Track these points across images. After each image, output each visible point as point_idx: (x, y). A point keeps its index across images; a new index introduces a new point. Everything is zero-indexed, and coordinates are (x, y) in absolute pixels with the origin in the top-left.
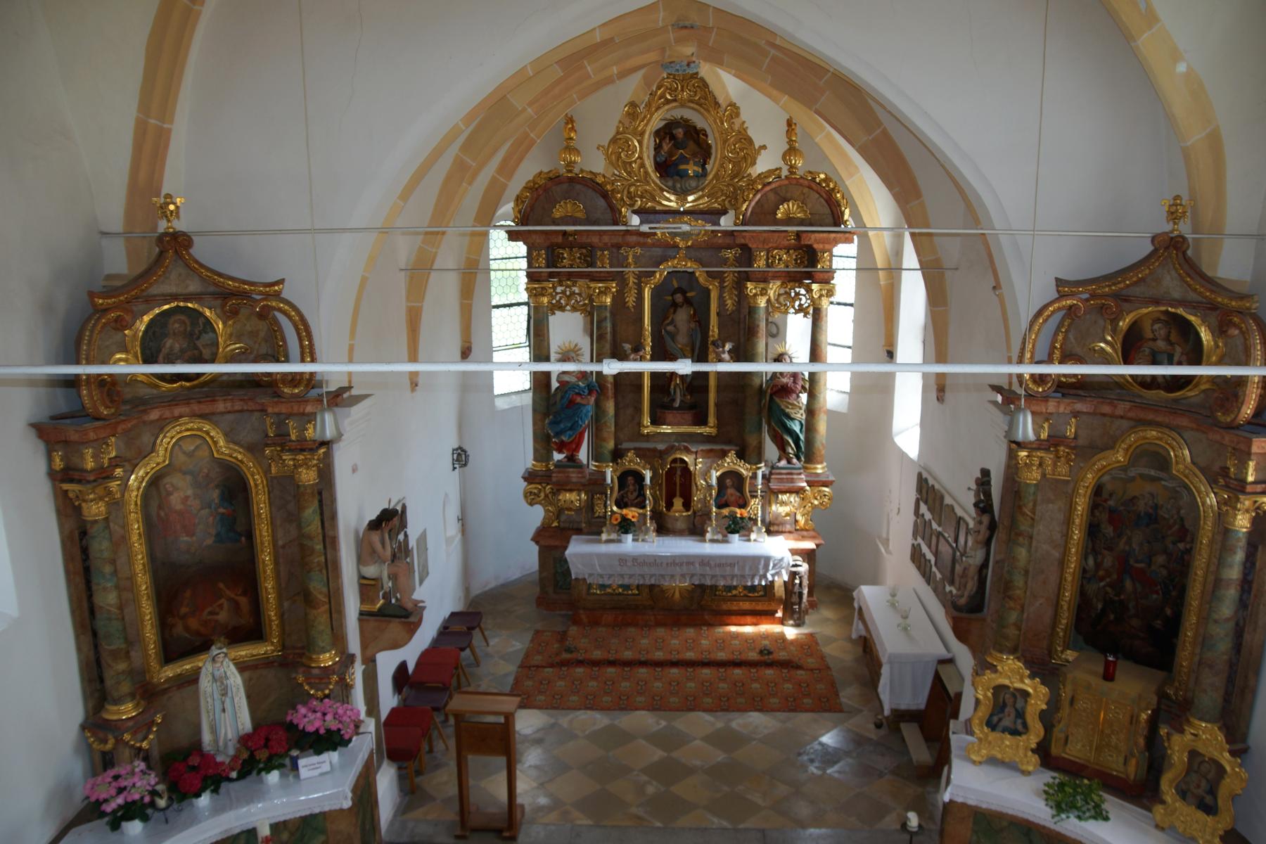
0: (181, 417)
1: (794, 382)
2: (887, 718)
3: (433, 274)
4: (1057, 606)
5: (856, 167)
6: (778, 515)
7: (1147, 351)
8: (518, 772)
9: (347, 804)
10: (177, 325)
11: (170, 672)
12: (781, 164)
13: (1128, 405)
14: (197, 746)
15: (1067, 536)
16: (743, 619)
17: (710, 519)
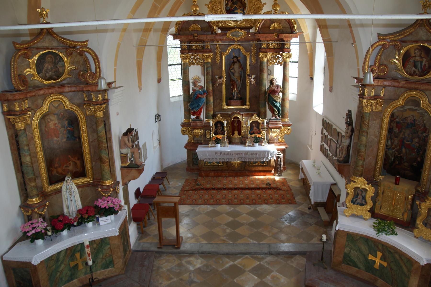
0: (52, 93)
1: (277, 88)
2: (312, 205)
3: (146, 47)
4: (377, 159)
5: (299, 9)
6: (272, 137)
7: (412, 61)
8: (180, 226)
9: (117, 234)
10: (49, 59)
11: (52, 188)
12: (272, 9)
13: (404, 82)
14: (63, 215)
15: (380, 133)
16: (260, 174)
17: (248, 138)
